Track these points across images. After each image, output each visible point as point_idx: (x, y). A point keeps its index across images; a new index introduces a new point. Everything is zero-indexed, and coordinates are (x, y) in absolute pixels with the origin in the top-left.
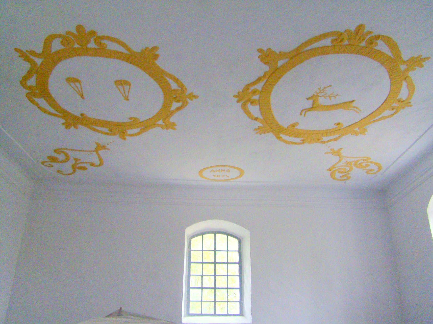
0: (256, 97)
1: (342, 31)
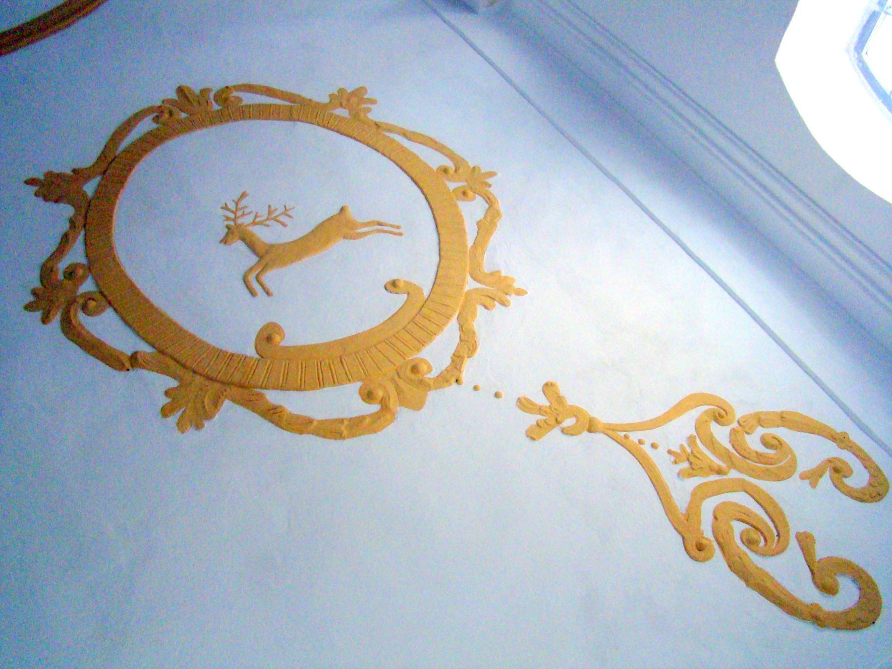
0: (88, 286)
1: (159, 103)
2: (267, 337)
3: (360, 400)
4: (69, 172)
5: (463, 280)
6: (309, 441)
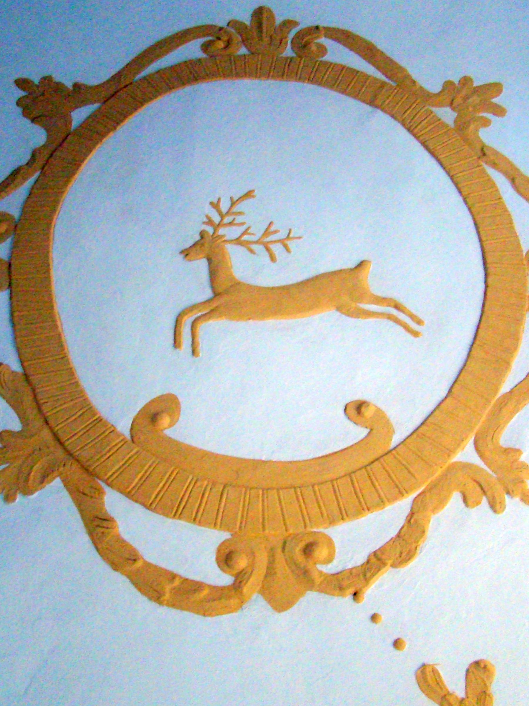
1: (222, 23)
2: (158, 411)
3: (214, 559)
4: (69, 85)
5: (459, 443)
6: (120, 584)
